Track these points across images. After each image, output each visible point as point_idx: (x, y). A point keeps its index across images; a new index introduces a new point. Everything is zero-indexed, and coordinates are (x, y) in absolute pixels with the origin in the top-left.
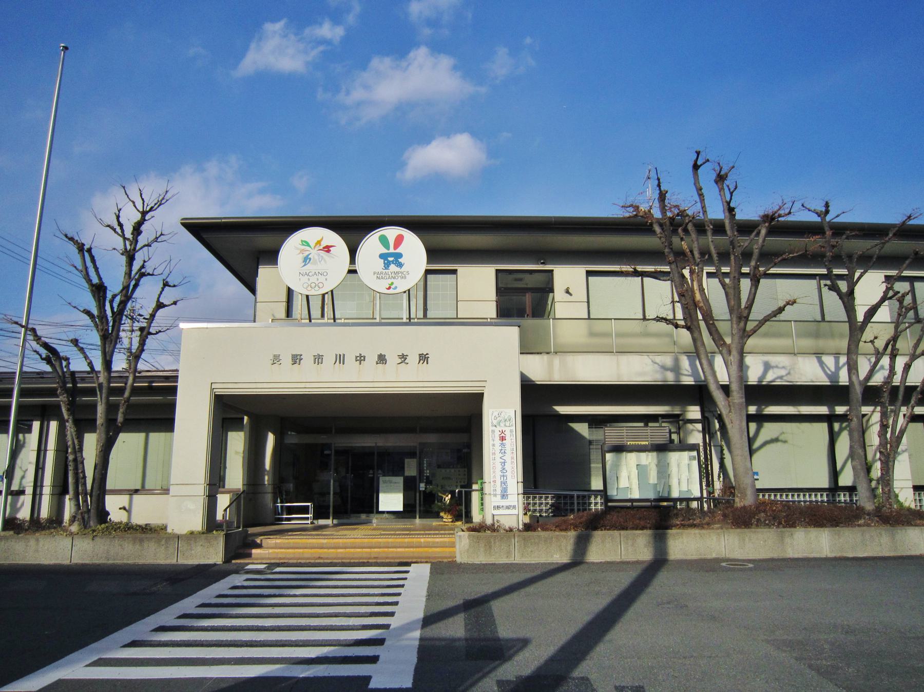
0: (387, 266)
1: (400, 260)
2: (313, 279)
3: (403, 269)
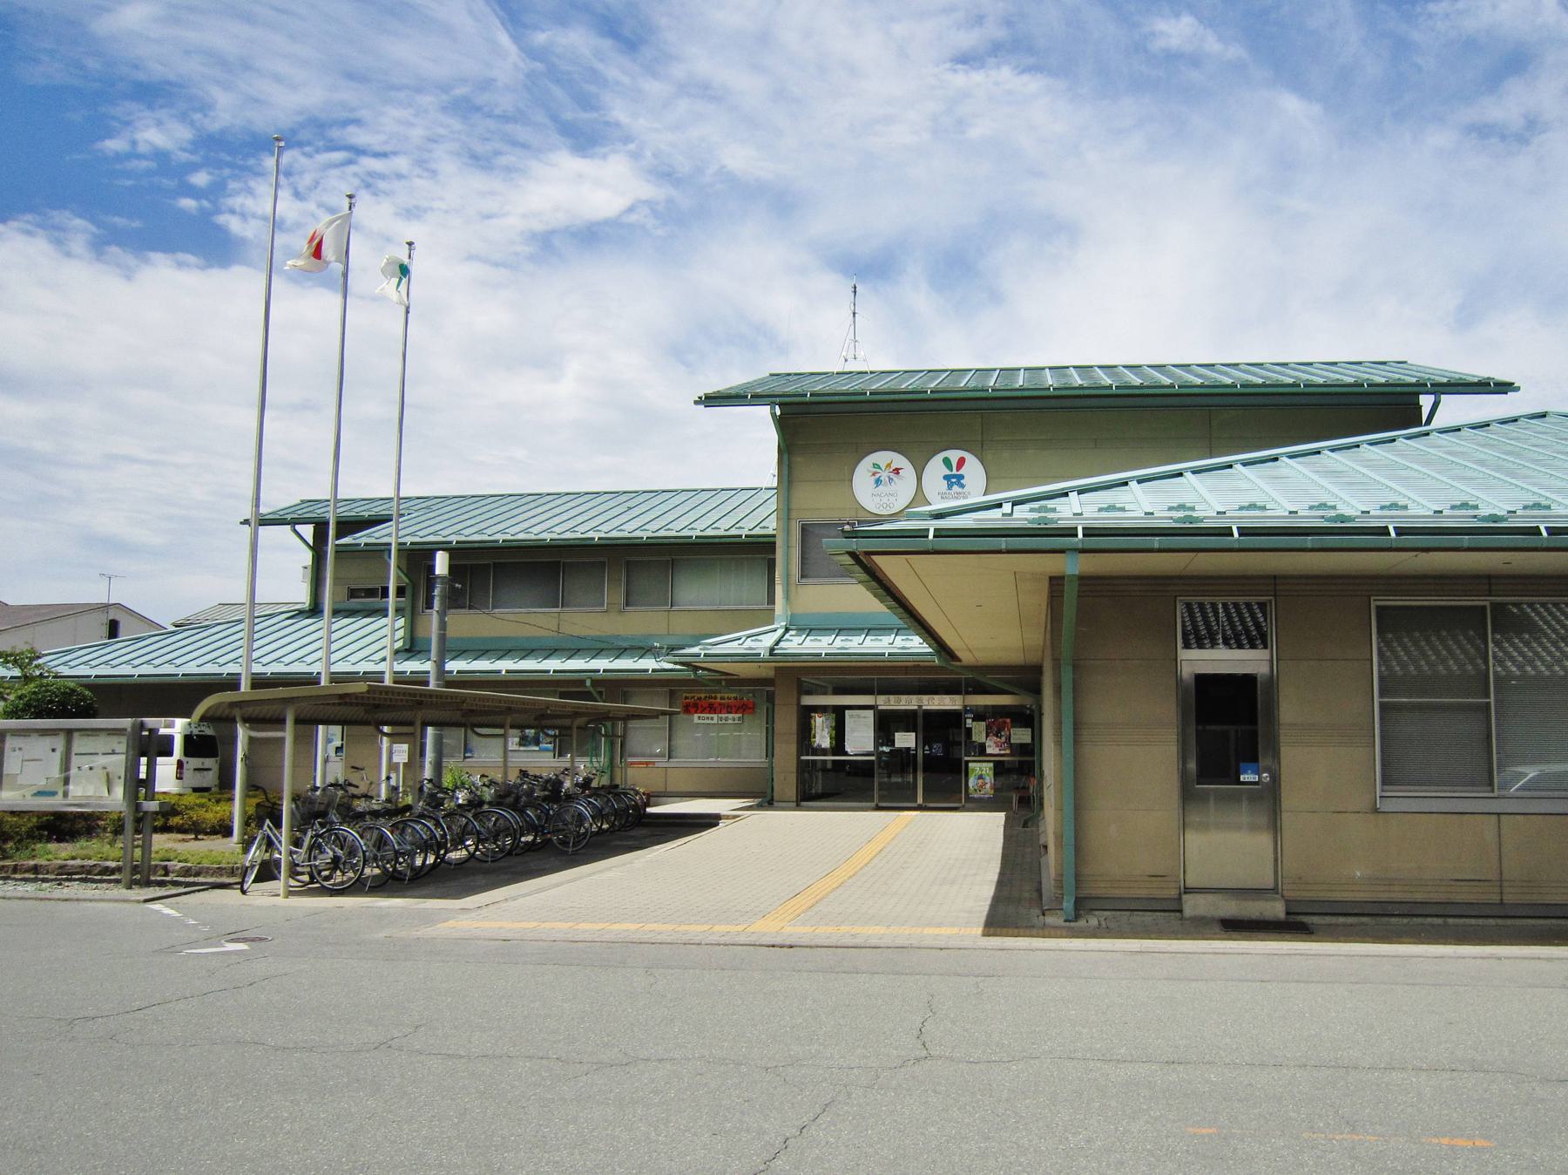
0: (950, 487)
2: (885, 500)
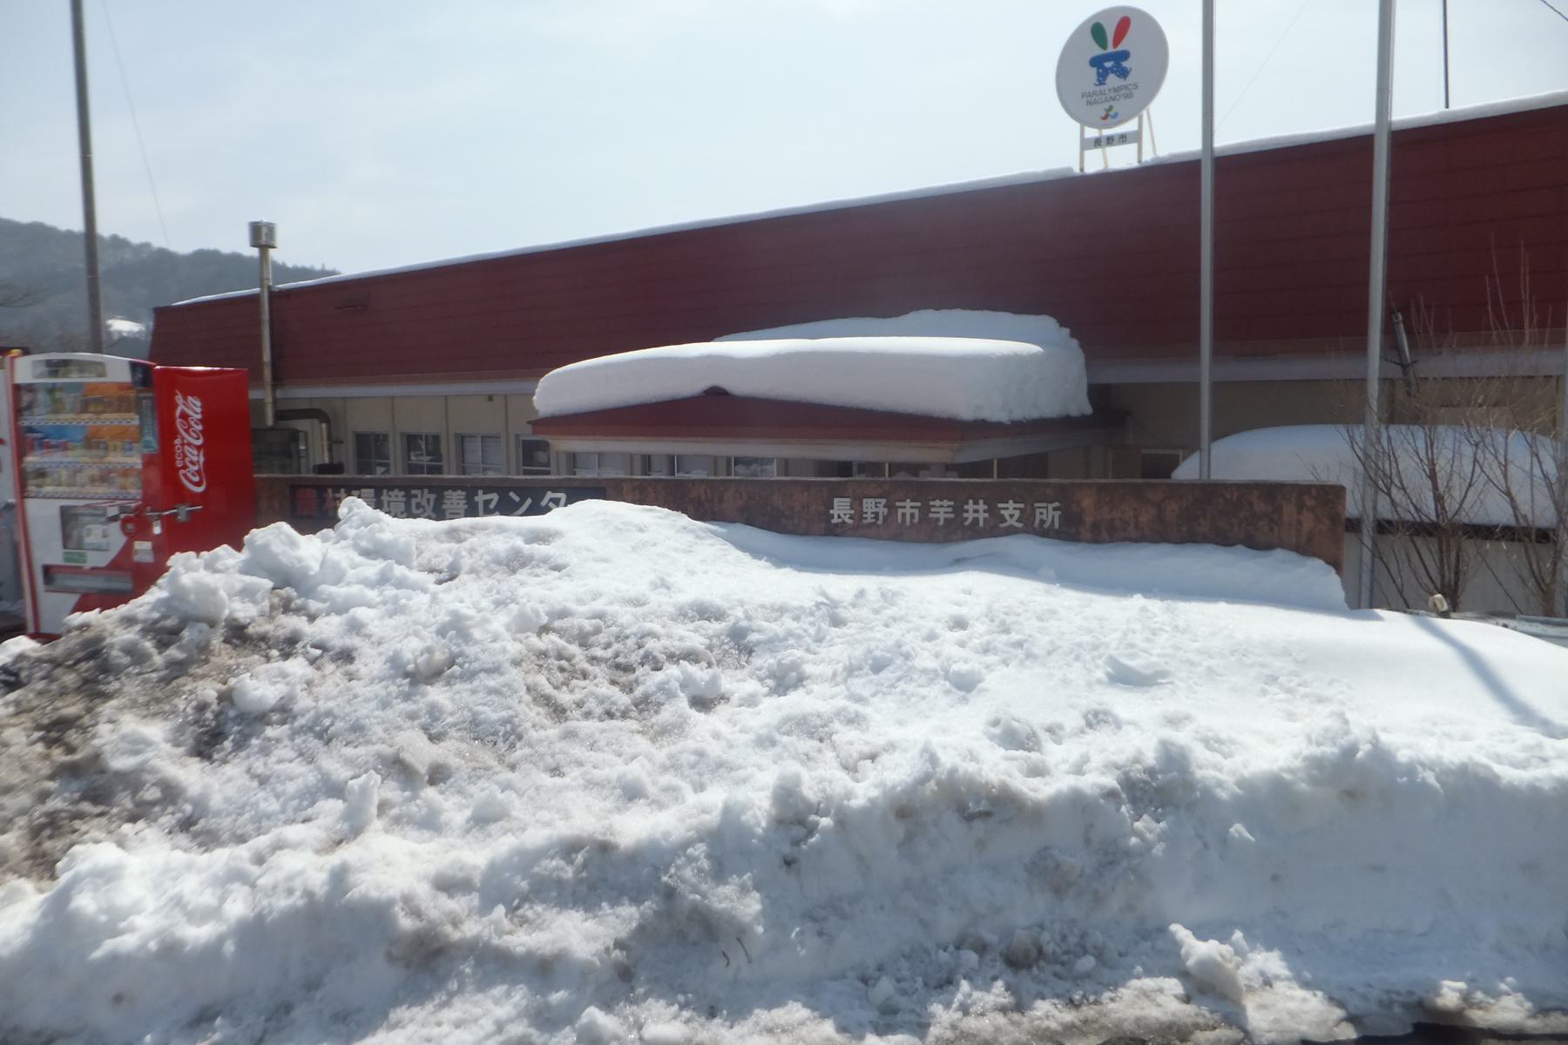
0: (1102, 78)
1: (1124, 64)
3: (1131, 79)
